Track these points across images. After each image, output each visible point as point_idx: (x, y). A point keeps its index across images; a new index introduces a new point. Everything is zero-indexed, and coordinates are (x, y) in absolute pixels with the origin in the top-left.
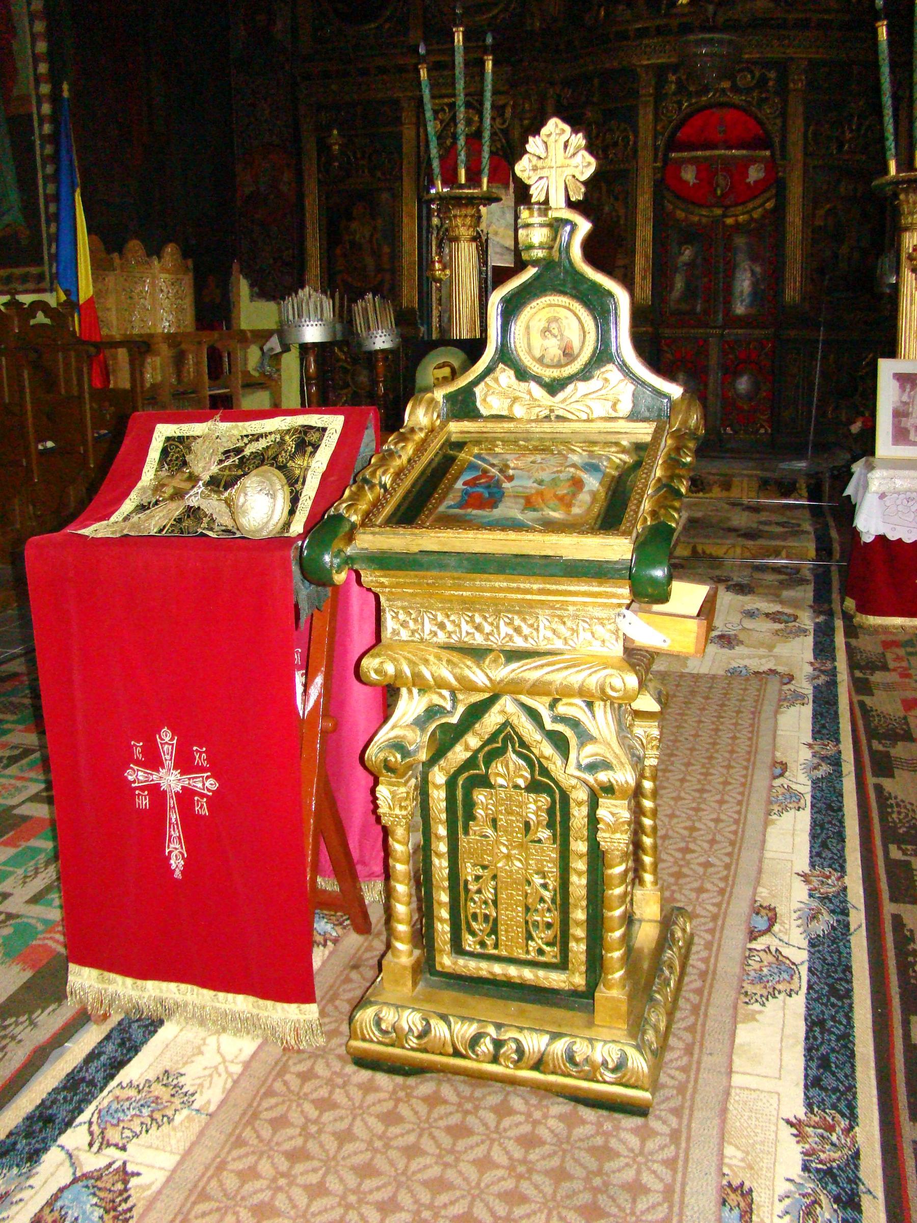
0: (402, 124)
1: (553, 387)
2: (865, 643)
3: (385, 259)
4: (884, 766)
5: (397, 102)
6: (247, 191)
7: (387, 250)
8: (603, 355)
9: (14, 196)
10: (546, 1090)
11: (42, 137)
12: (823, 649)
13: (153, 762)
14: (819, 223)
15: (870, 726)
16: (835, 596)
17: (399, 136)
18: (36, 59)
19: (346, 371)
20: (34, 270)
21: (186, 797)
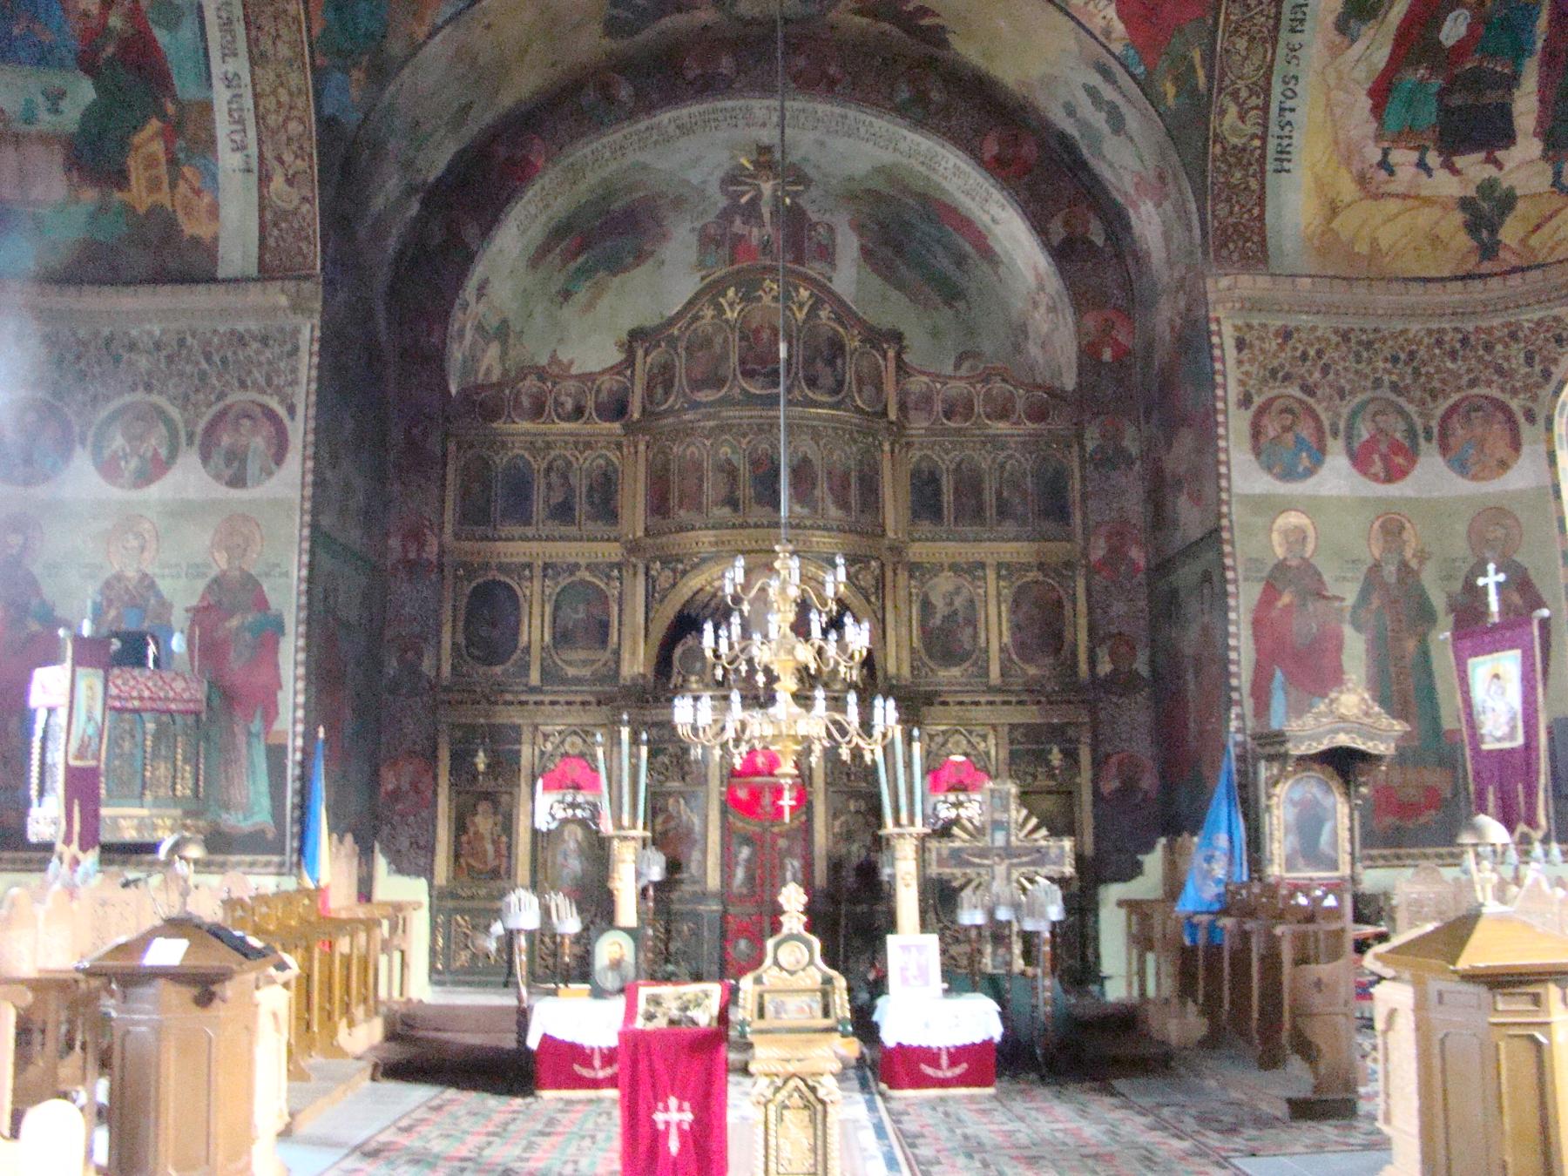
0: (520, 743)
1: (792, 973)
2: (894, 1105)
3: (503, 847)
4: (912, 1146)
5: (519, 726)
6: (390, 787)
7: (504, 839)
8: (811, 962)
9: (265, 802)
10: (1243, 787)
11: (294, 762)
12: (872, 1107)
13: (666, 1109)
14: (837, 830)
15: (902, 1134)
16: (872, 1084)
17: (518, 753)
18: (296, 706)
19: (466, 935)
20: (276, 859)
21: (679, 1125)
